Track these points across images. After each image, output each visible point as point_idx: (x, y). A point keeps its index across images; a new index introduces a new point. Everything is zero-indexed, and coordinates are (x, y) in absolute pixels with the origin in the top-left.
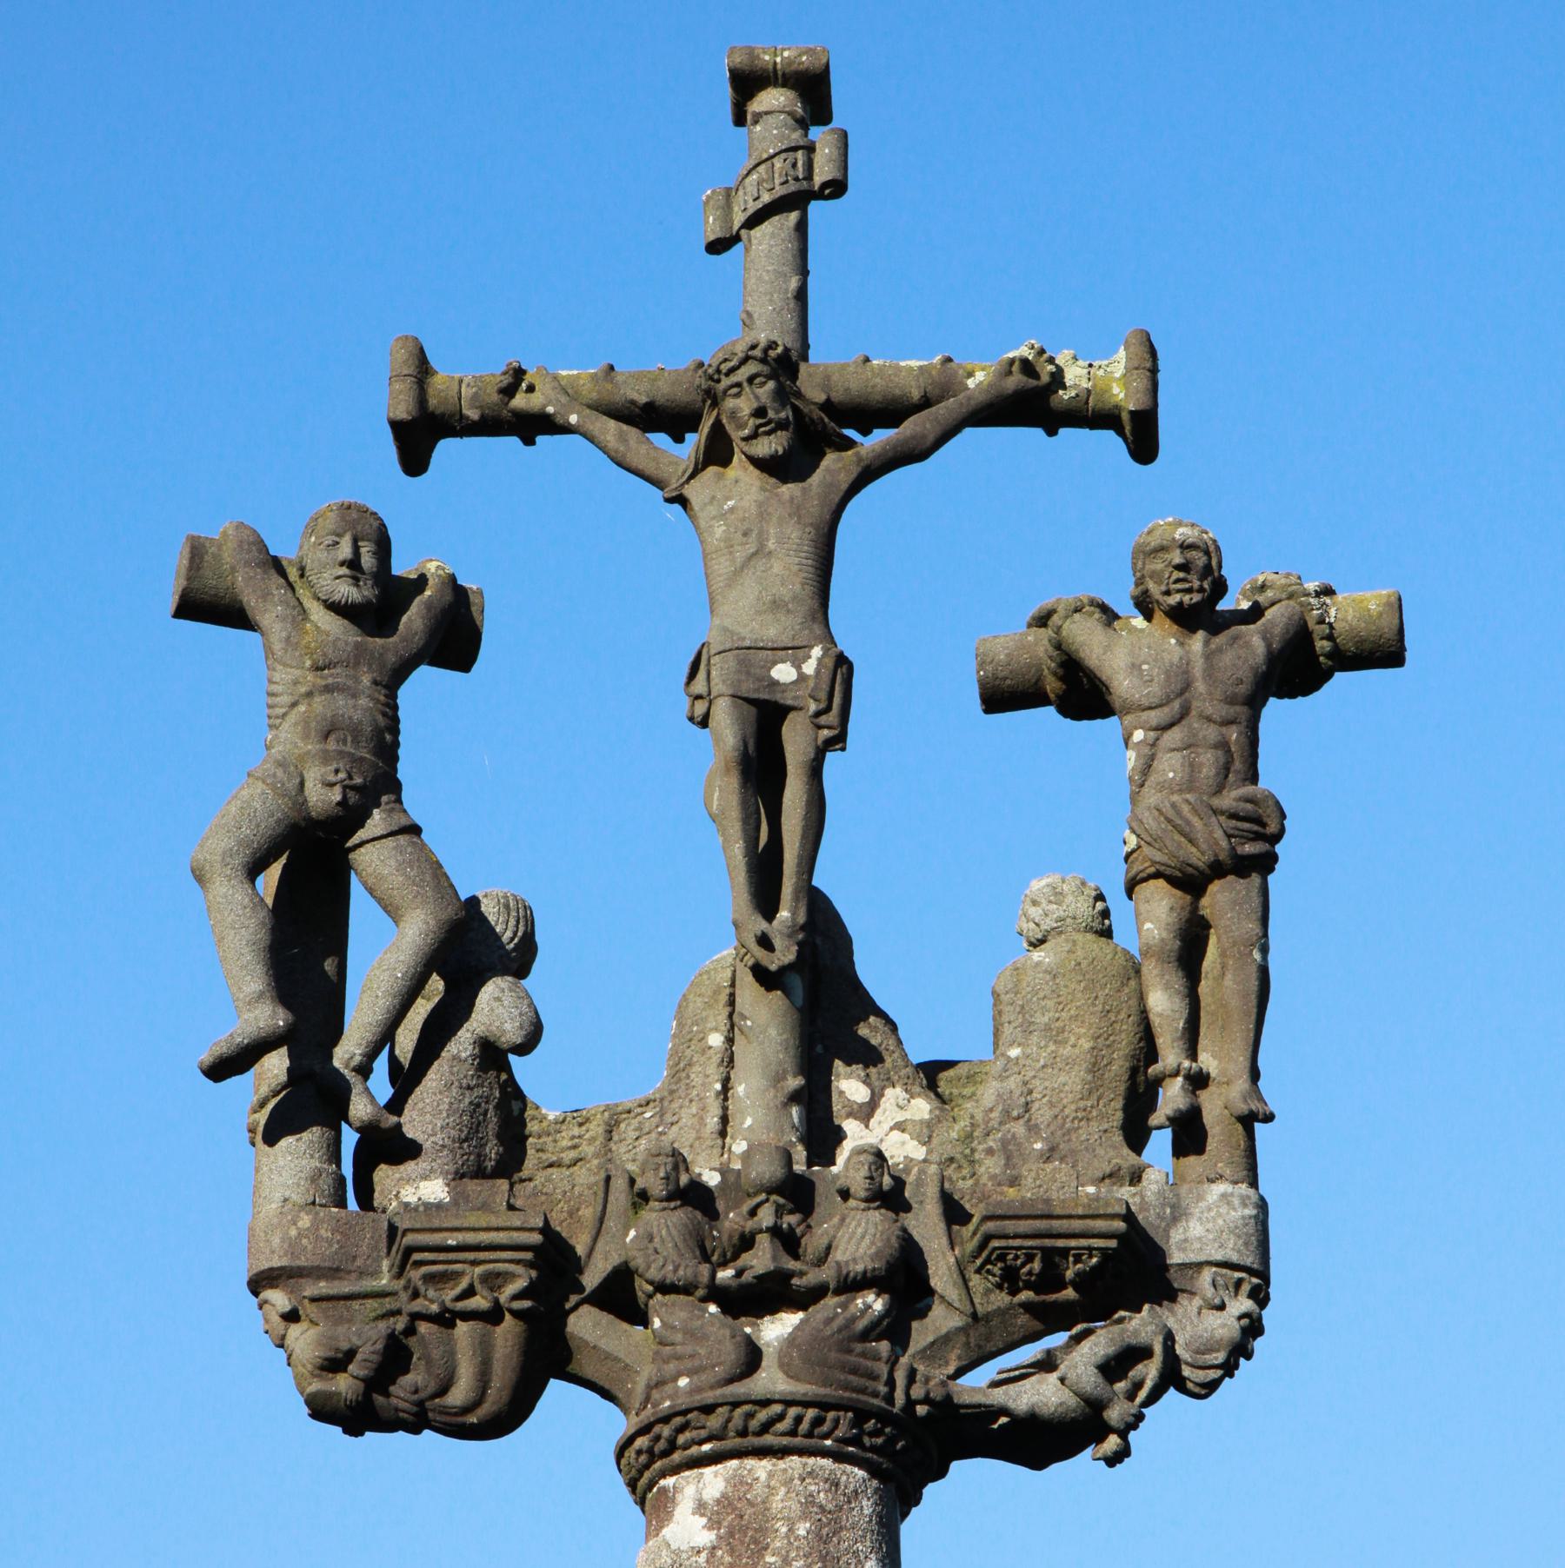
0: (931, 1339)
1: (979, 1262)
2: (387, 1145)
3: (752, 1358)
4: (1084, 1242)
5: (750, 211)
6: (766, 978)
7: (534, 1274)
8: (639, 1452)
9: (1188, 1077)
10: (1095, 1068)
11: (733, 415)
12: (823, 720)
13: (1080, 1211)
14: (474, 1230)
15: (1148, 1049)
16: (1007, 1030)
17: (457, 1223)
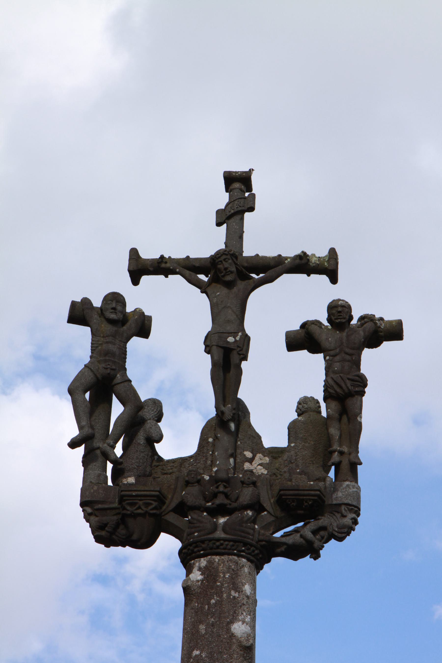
0: (265, 523)
3: (215, 527)
4: (308, 497)
13: (307, 488)
17: (135, 489)
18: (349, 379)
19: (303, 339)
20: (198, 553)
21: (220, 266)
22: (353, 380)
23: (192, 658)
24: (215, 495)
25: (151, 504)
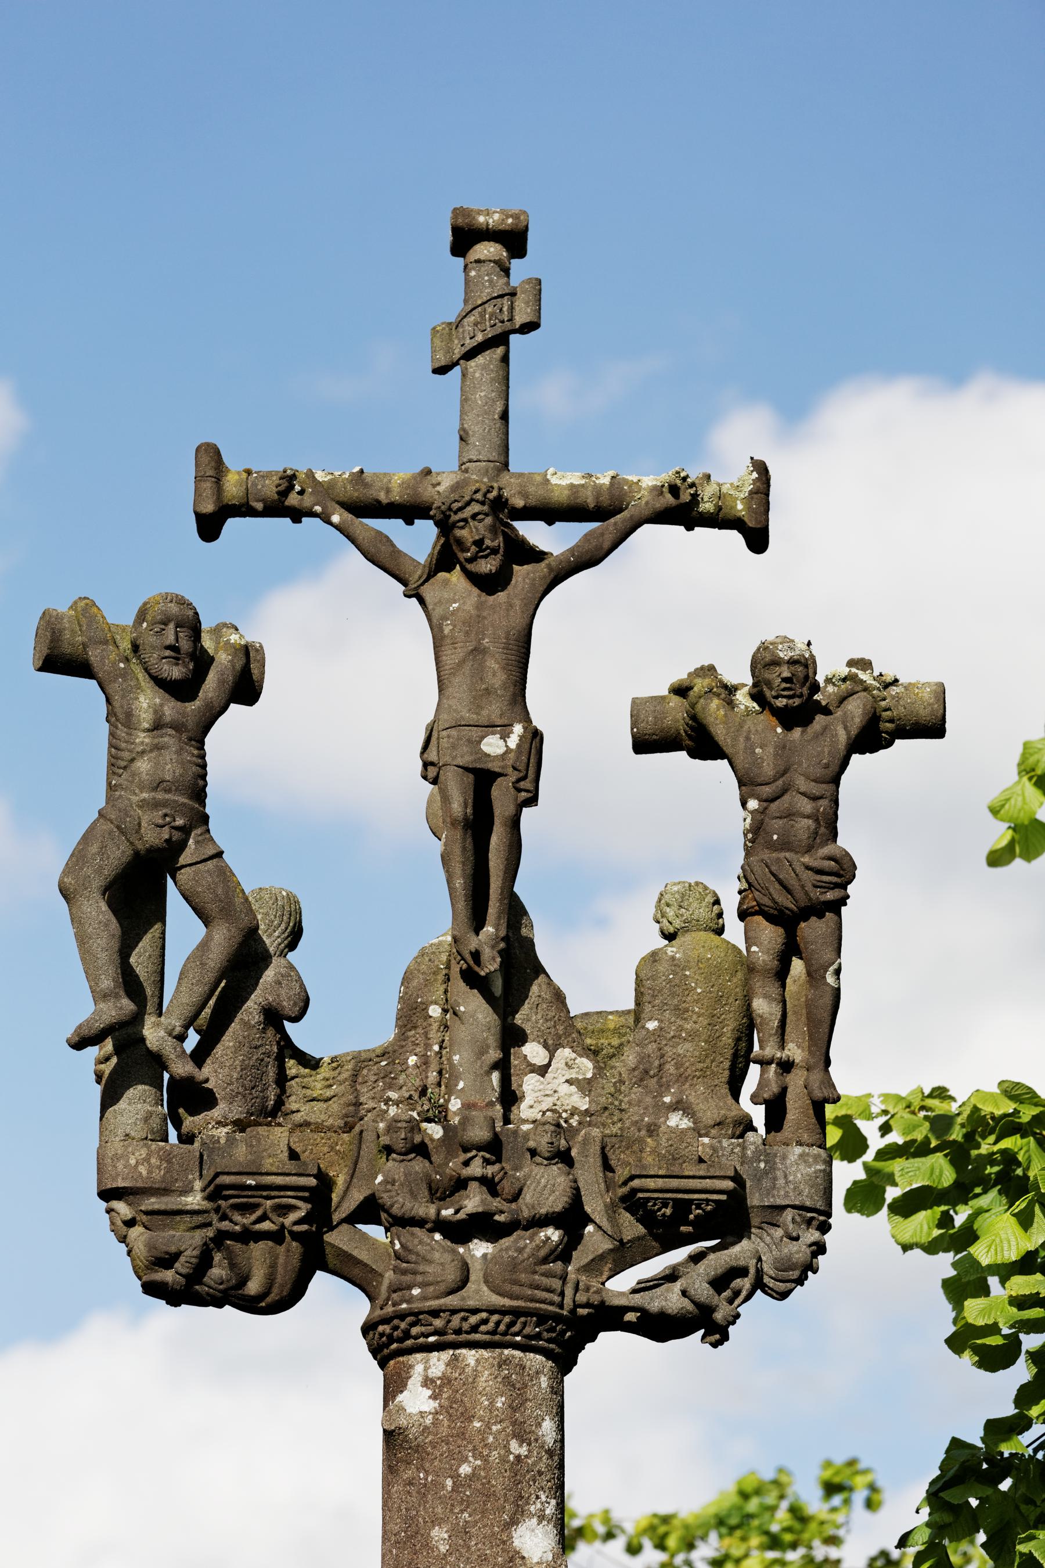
0: (591, 1257)
2: (191, 1097)
5: (468, 348)
7: (309, 1206)
8: (382, 1335)
10: (713, 1041)
12: (522, 785)
16: (648, 1008)
18: (808, 868)
19: (678, 728)
20: (422, 1340)
21: (463, 533)
22: (820, 872)
24: (461, 1184)
25: (294, 1208)
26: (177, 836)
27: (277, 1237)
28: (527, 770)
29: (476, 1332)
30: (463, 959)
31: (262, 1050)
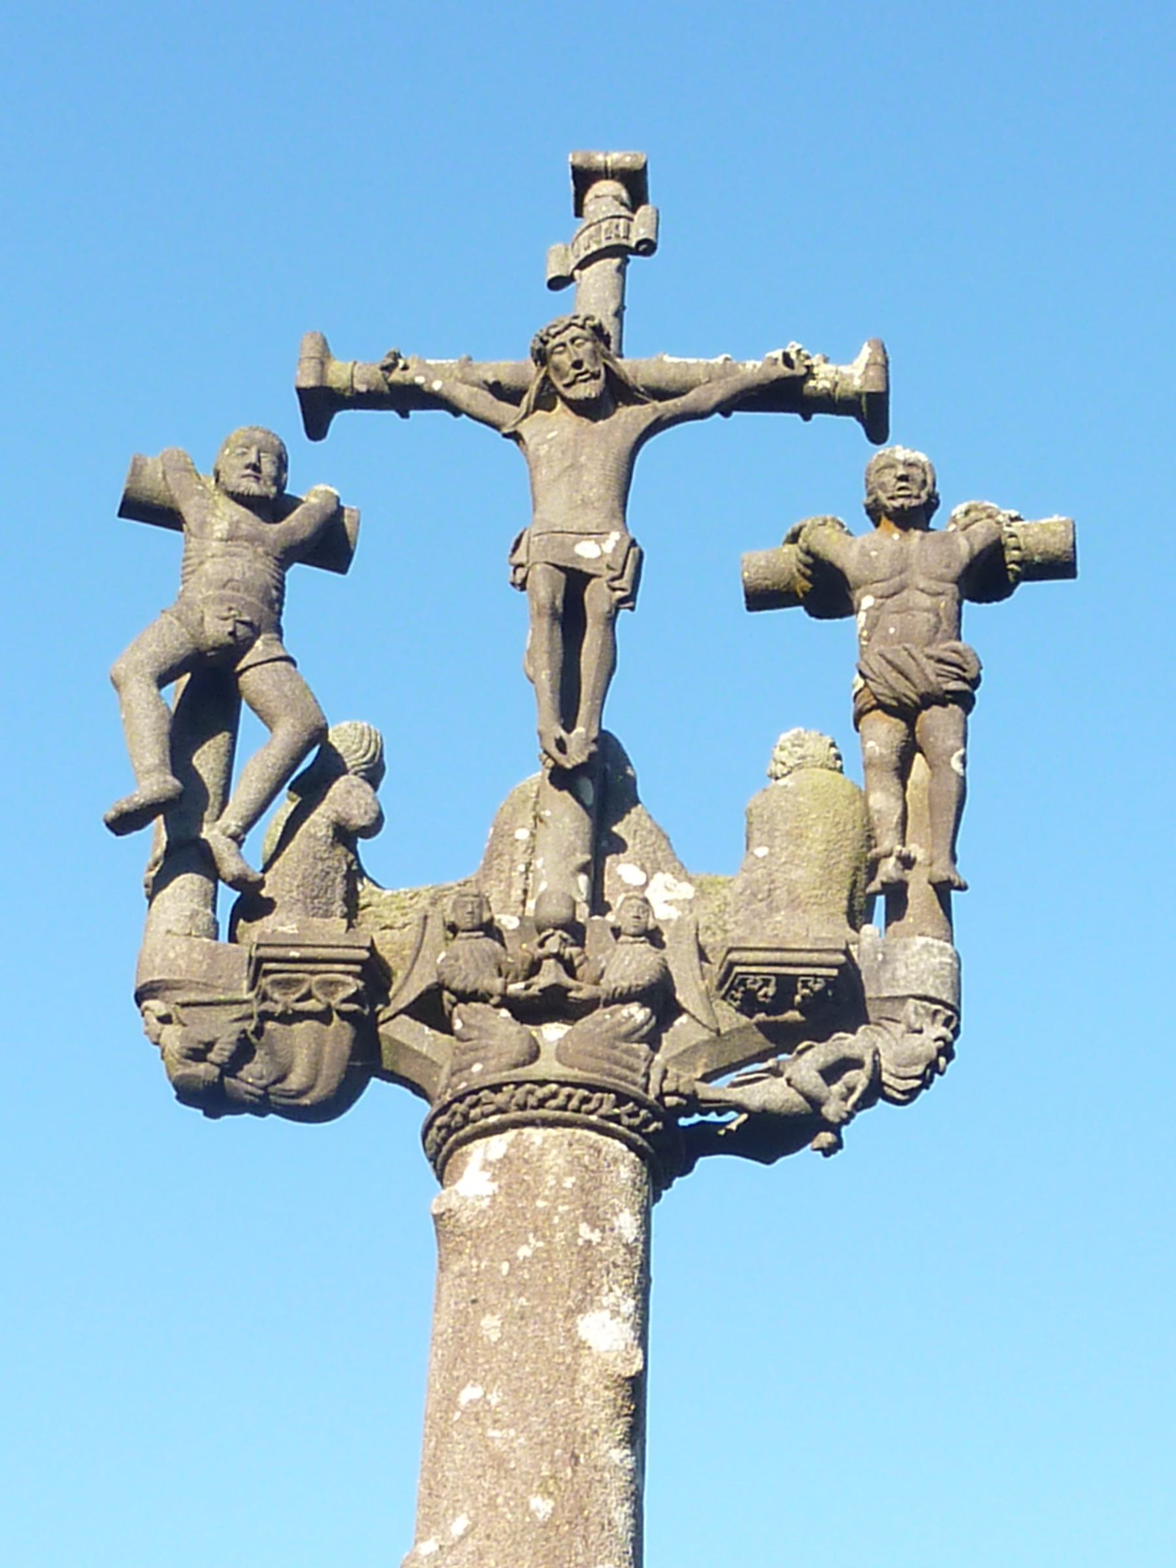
0: (682, 1048)
1: (723, 992)
2: (253, 904)
5: (582, 257)
6: (561, 778)
7: (361, 984)
8: (440, 1128)
9: (899, 858)
10: (827, 868)
11: (557, 369)
12: (616, 584)
14: (314, 946)
15: (870, 839)
16: (756, 835)
18: (930, 657)
22: (940, 661)
23: (458, 1409)
24: (535, 967)
25: (344, 984)
26: (242, 631)
27: (324, 1017)
28: (624, 568)
29: (543, 1107)
30: (550, 756)
31: (329, 863)
